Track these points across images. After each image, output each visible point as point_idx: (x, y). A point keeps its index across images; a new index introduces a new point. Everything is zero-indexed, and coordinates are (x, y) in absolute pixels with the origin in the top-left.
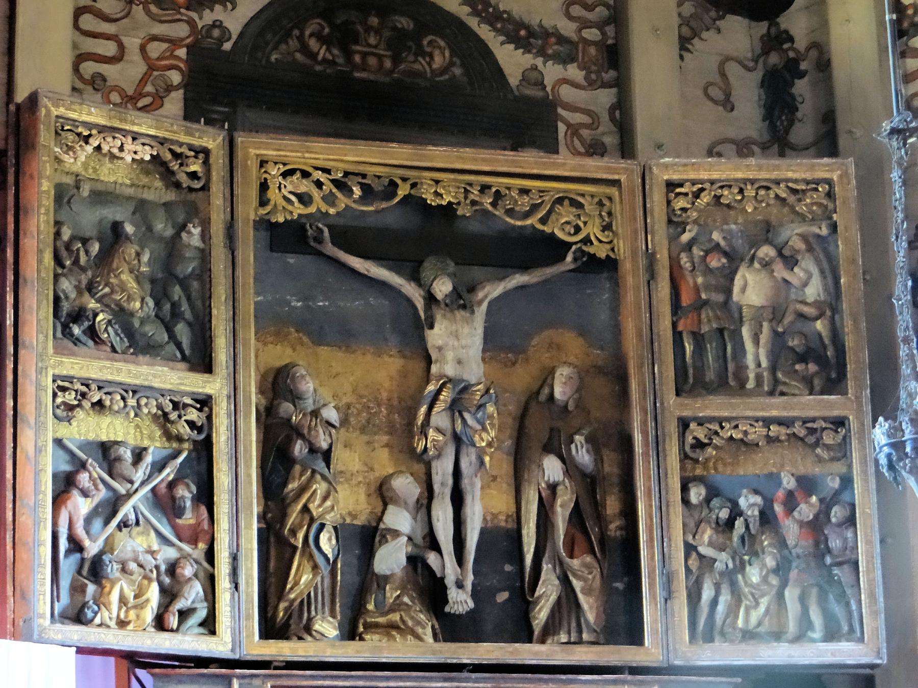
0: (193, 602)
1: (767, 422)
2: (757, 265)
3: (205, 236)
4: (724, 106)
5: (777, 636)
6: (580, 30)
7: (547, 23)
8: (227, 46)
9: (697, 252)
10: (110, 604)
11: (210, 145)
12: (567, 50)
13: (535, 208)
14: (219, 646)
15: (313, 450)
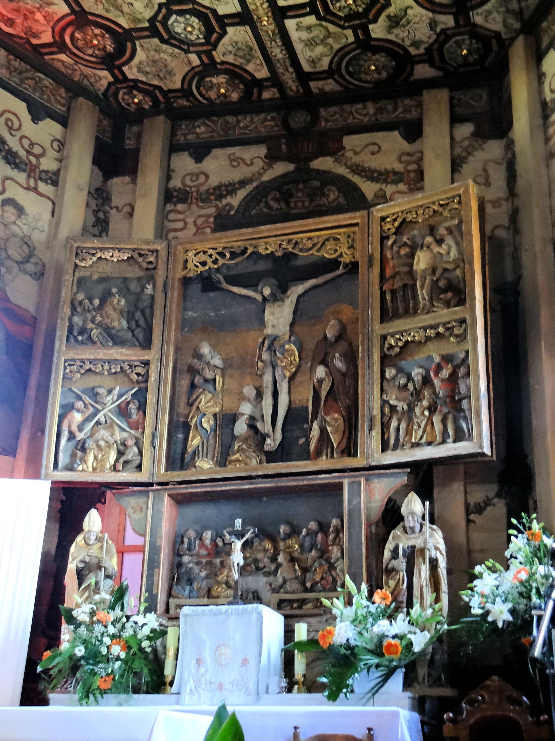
0: (133, 456)
1: (425, 329)
2: (425, 248)
3: (154, 288)
4: (485, 185)
5: (429, 444)
6: (406, 167)
7: (389, 167)
8: (232, 213)
9: (395, 248)
10: (88, 460)
11: (159, 248)
12: (396, 177)
13: (314, 245)
14: (143, 477)
15: (206, 380)
